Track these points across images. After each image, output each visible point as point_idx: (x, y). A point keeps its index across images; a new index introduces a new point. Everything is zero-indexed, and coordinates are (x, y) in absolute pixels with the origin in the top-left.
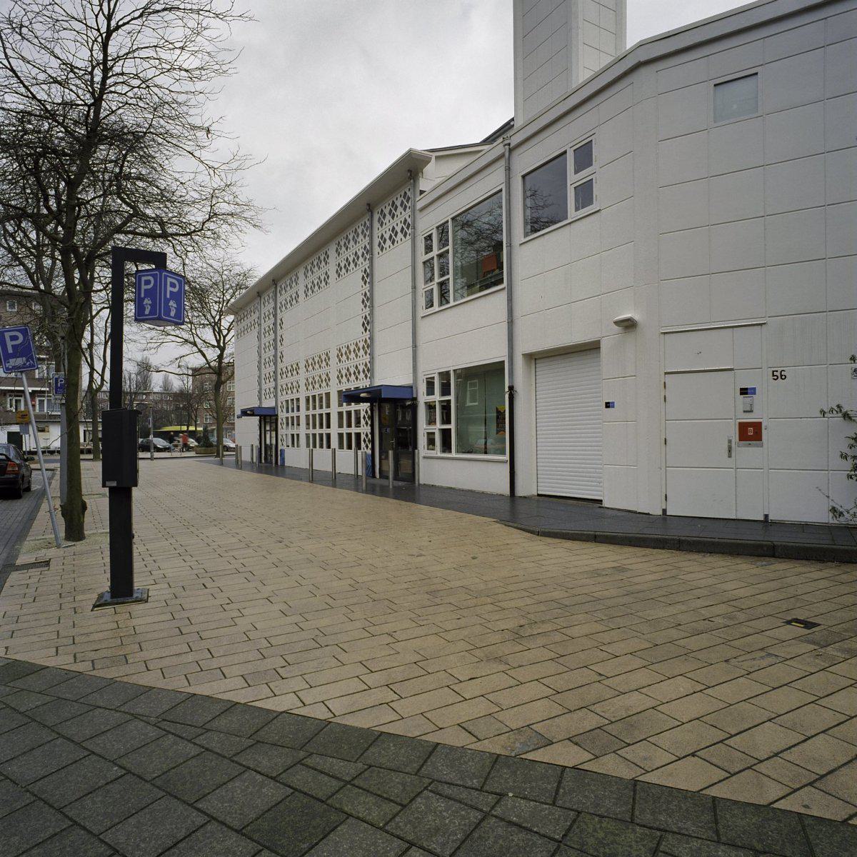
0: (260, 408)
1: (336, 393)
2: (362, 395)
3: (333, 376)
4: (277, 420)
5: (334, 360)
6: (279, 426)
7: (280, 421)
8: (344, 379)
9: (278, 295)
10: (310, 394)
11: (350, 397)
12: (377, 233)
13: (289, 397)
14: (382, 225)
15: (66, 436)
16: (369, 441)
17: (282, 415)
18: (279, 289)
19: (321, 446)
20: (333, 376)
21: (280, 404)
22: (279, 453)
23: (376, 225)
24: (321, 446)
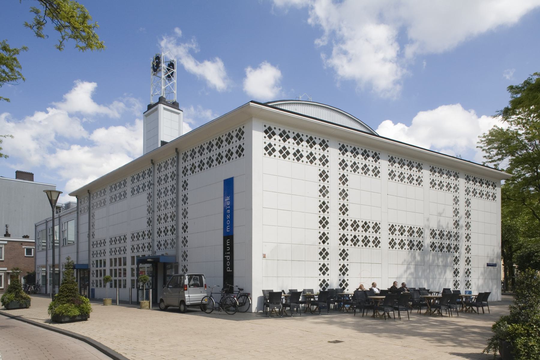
0: (77, 264)
1: (130, 258)
2: (148, 260)
3: (108, 251)
4: (89, 271)
5: (108, 243)
6: (91, 275)
7: (91, 272)
8: (113, 253)
9: (92, 199)
10: (113, 257)
11: (142, 260)
12: (182, 165)
13: (99, 259)
14: (185, 161)
15: (381, 335)
16: (150, 284)
17: (93, 269)
18: (92, 195)
19: (101, 286)
20: (108, 251)
21: (91, 262)
22: (91, 291)
23: (181, 161)
24: (101, 286)
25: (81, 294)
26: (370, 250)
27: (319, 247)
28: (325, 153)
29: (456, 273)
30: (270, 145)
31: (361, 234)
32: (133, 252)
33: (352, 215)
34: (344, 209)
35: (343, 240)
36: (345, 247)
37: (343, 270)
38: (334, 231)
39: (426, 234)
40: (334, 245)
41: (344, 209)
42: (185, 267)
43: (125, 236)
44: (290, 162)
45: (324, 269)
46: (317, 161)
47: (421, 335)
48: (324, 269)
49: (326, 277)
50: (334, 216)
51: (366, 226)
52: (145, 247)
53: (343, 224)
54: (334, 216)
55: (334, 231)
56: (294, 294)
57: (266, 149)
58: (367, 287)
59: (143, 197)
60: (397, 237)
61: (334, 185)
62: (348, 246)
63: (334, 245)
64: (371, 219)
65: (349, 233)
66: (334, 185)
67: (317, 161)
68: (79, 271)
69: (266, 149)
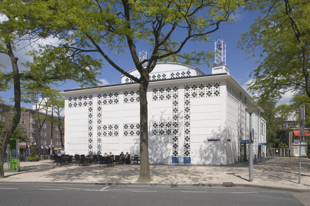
26: (113, 138)
27: (88, 138)
28: (117, 98)
29: (175, 146)
30: (160, 97)
35: (99, 134)
37: (99, 147)
38: (95, 132)
39: (180, 128)
40: (95, 137)
44: (78, 108)
45: (90, 147)
47: (253, 186)
48: (90, 147)
49: (91, 150)
50: (95, 125)
51: (111, 127)
53: (99, 128)
54: (95, 125)
56: (77, 156)
57: (217, 95)
60: (113, 130)
61: (95, 112)
64: (113, 123)
66: (95, 112)
68: (181, 154)
69: (217, 95)
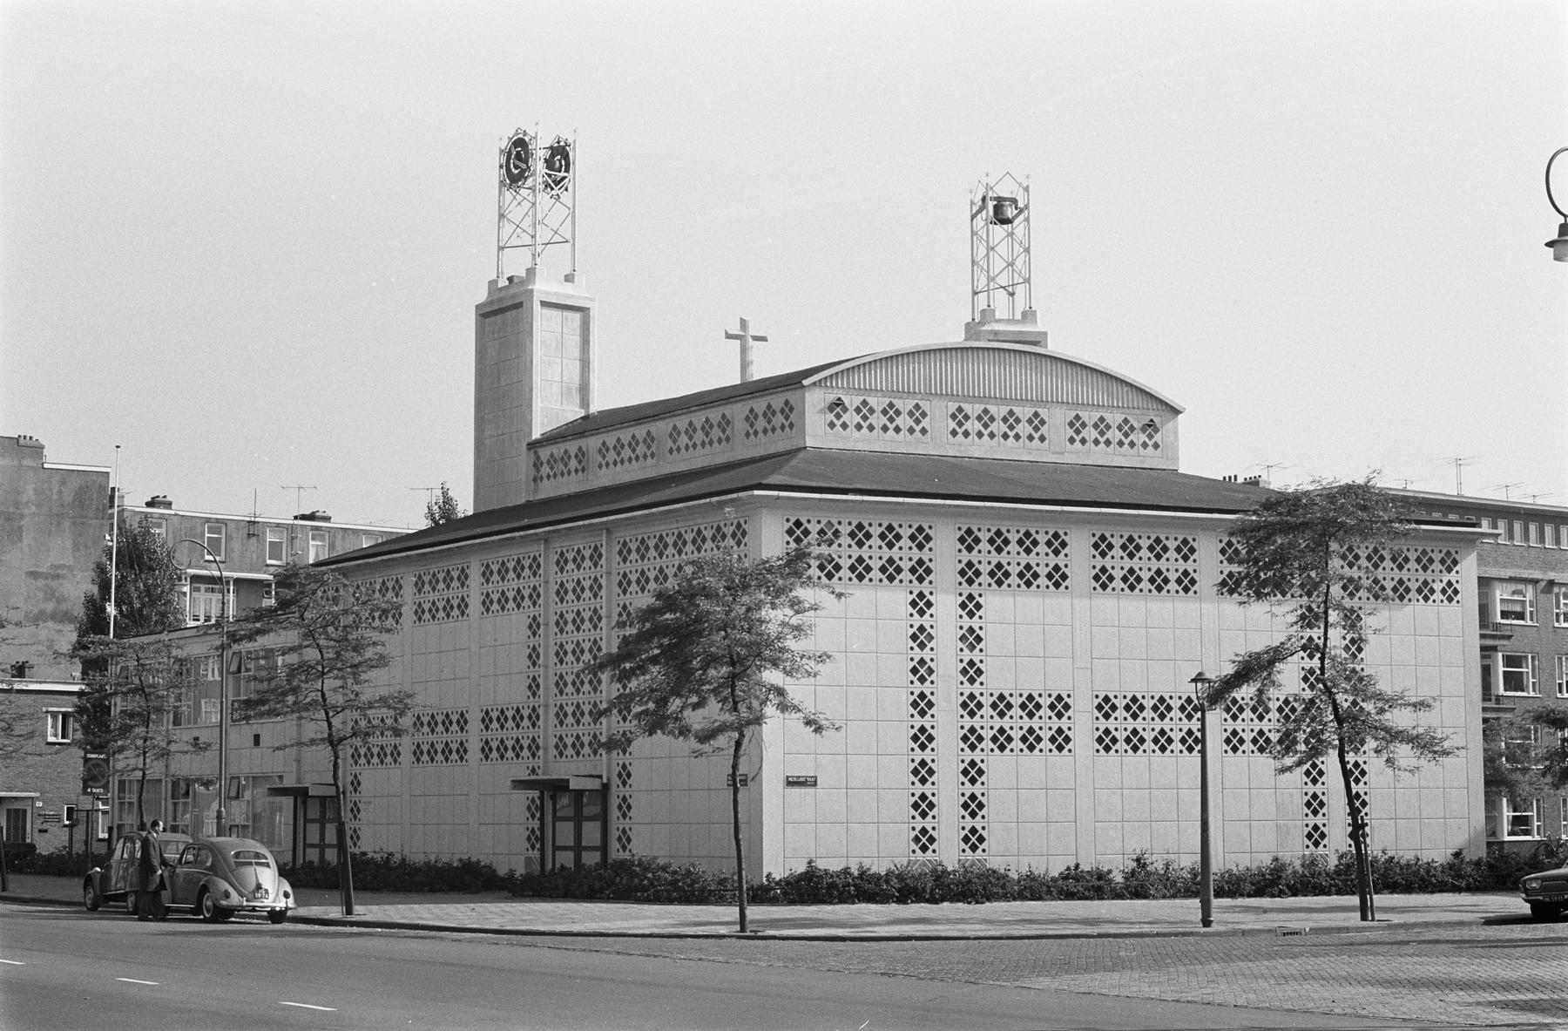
25: (1303, 569)
31: (1036, 722)
32: (487, 728)
33: (995, 680)
34: (972, 672)
35: (971, 739)
36: (977, 756)
38: (947, 723)
40: (948, 755)
41: (972, 672)
42: (624, 799)
43: (418, 760)
46: (906, 575)
50: (947, 689)
52: (491, 750)
53: (971, 706)
54: (947, 689)
55: (947, 723)
58: (474, 859)
59: (515, 621)
62: (987, 756)
63: (948, 755)
65: (987, 722)
67: (906, 575)
